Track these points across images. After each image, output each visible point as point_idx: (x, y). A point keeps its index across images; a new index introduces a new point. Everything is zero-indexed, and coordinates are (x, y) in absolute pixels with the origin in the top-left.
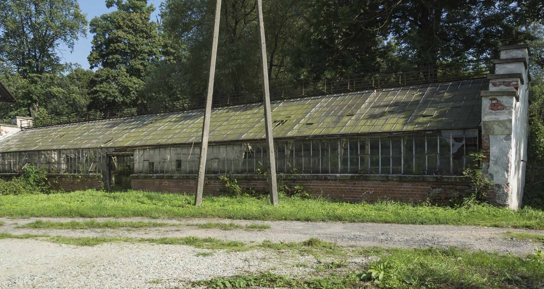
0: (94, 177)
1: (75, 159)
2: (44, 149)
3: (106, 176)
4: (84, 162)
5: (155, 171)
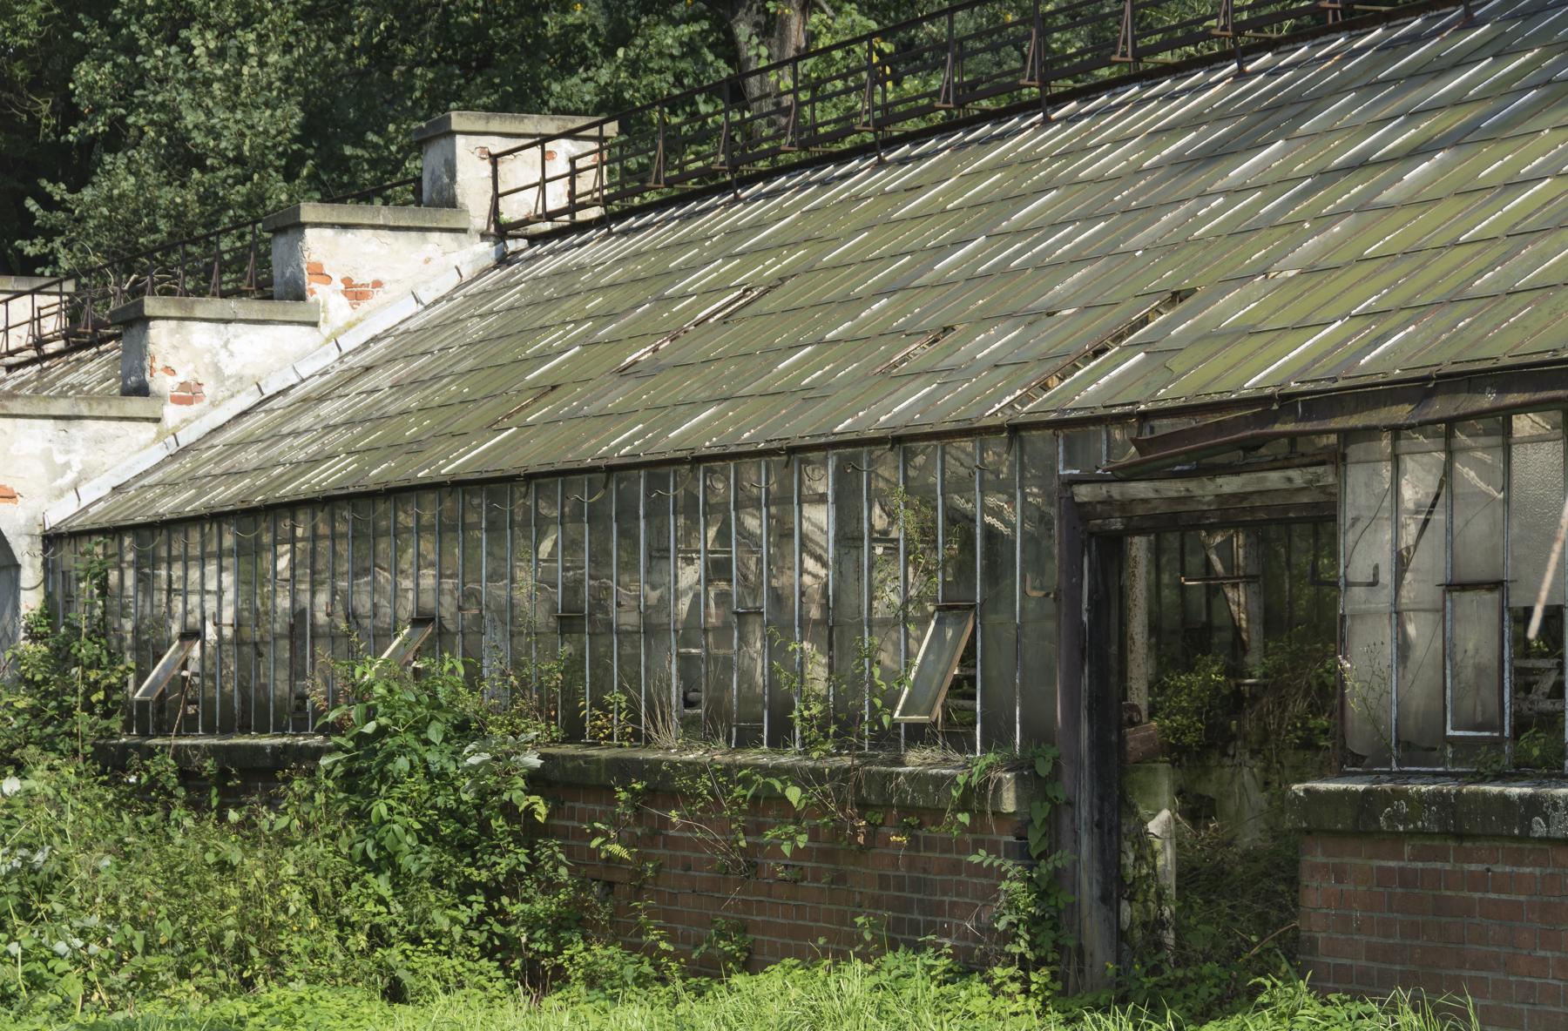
3: (1061, 792)
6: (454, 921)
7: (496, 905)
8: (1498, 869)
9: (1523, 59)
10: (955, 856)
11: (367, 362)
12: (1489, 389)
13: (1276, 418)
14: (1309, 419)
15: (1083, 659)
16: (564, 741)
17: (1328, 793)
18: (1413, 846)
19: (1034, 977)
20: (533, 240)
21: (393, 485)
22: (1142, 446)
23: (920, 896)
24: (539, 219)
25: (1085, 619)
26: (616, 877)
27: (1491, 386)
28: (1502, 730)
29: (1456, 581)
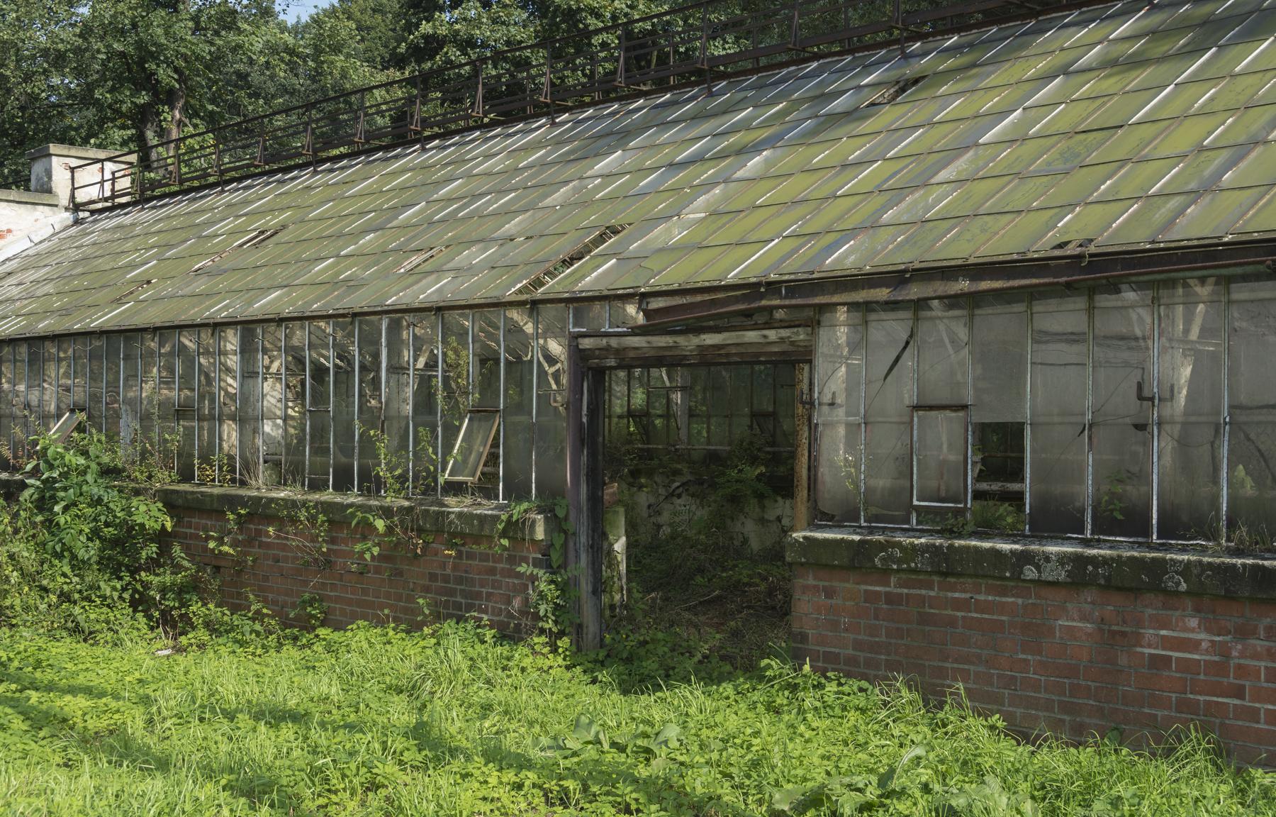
0: (478, 529)
1: (344, 374)
2: (158, 322)
4: (409, 409)
5: (1038, 509)
6: (114, 589)
7: (138, 577)
8: (982, 597)
9: (778, 108)
10: (491, 564)
11: (9, 270)
12: (961, 278)
13: (762, 296)
14: (792, 298)
15: (583, 445)
16: (179, 482)
17: (826, 541)
18: (899, 579)
19: (559, 643)
20: (93, 212)
21: (57, 333)
22: (647, 314)
23: (463, 587)
24: (100, 200)
25: (584, 420)
26: (222, 564)
27: (964, 276)
28: (966, 503)
29: (921, 403)
